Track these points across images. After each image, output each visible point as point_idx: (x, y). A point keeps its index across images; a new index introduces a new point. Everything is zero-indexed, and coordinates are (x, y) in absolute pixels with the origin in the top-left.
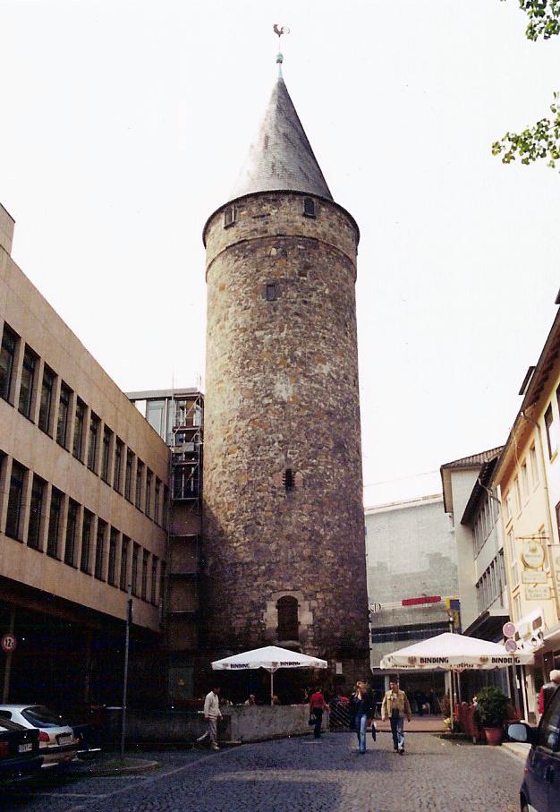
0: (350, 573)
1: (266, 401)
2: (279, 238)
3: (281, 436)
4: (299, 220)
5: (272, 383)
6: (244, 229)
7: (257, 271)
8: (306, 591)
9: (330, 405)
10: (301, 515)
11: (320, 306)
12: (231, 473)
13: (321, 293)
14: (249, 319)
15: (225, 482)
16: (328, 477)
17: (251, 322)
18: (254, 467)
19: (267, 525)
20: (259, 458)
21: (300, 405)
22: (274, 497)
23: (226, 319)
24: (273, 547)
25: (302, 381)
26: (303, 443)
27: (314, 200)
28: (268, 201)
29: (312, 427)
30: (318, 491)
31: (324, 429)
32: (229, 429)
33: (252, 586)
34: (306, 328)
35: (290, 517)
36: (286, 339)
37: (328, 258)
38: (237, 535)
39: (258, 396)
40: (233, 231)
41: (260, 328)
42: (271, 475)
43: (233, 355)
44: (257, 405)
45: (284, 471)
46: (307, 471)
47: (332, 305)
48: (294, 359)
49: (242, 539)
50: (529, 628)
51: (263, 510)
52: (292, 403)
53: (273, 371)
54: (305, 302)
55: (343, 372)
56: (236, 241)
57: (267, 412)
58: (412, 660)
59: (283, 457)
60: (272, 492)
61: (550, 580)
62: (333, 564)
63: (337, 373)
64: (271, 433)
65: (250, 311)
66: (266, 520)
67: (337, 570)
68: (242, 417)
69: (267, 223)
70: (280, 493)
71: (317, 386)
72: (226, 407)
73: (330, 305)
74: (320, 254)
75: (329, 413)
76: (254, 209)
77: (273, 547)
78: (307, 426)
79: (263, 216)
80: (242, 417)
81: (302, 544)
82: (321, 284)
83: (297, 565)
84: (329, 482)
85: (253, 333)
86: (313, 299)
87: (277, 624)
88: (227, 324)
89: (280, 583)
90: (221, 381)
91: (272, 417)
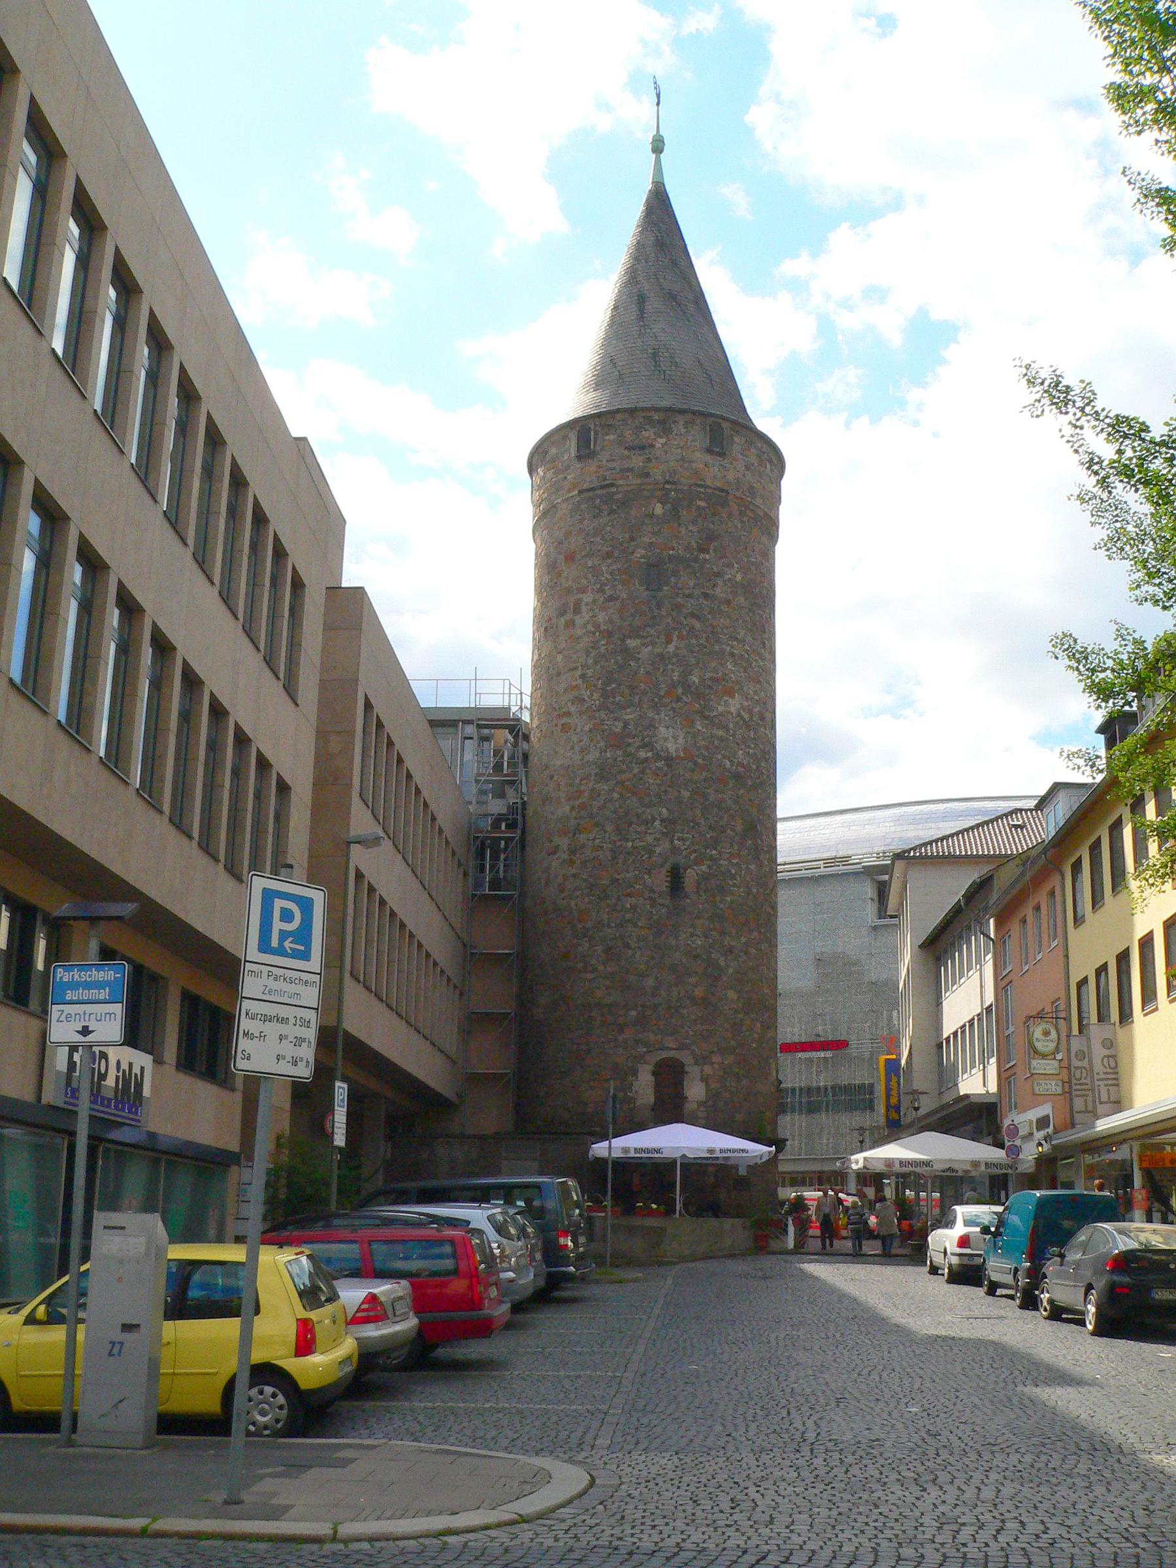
0: (758, 1025)
1: (643, 754)
2: (667, 486)
3: (664, 810)
4: (700, 457)
5: (652, 726)
6: (610, 465)
7: (632, 539)
8: (698, 1052)
9: (740, 764)
10: (692, 935)
11: (728, 602)
12: (584, 863)
13: (730, 579)
14: (616, 617)
15: (574, 876)
16: (733, 877)
17: (618, 622)
18: (622, 856)
19: (640, 948)
20: (630, 844)
21: (696, 763)
22: (652, 906)
23: (577, 610)
24: (650, 982)
25: (699, 726)
26: (698, 824)
27: (725, 425)
28: (650, 421)
29: (712, 798)
30: (718, 899)
31: (730, 802)
32: (581, 792)
33: (616, 1040)
34: (707, 638)
35: (676, 938)
36: (676, 655)
37: (742, 522)
38: (593, 962)
39: (629, 745)
40: (592, 466)
41: (635, 633)
42: (649, 873)
43: (590, 673)
44: (628, 759)
45: (668, 866)
46: (704, 868)
47: (746, 599)
48: (687, 687)
49: (601, 968)
50: (1031, 1127)
51: (635, 925)
52: (683, 759)
53: (655, 707)
54: (706, 596)
55: (757, 709)
56: (596, 484)
57: (643, 772)
58: (626, 1150)
59: (667, 845)
60: (650, 899)
61: (1065, 1071)
62: (737, 1012)
63: (750, 711)
64: (649, 805)
65: (618, 604)
66: (639, 941)
67: (741, 1020)
68: (602, 777)
69: (649, 460)
70: (661, 901)
71: (721, 733)
72: (577, 757)
73: (742, 599)
74: (730, 514)
75: (737, 777)
76: (627, 433)
77: (650, 982)
78: (705, 796)
79: (643, 448)
80: (602, 777)
81: (693, 980)
82: (730, 565)
83: (684, 1012)
84: (734, 885)
85: (623, 641)
86: (718, 590)
87: (652, 1100)
88: (579, 621)
89: (659, 1037)
90: (568, 714)
91: (651, 781)
